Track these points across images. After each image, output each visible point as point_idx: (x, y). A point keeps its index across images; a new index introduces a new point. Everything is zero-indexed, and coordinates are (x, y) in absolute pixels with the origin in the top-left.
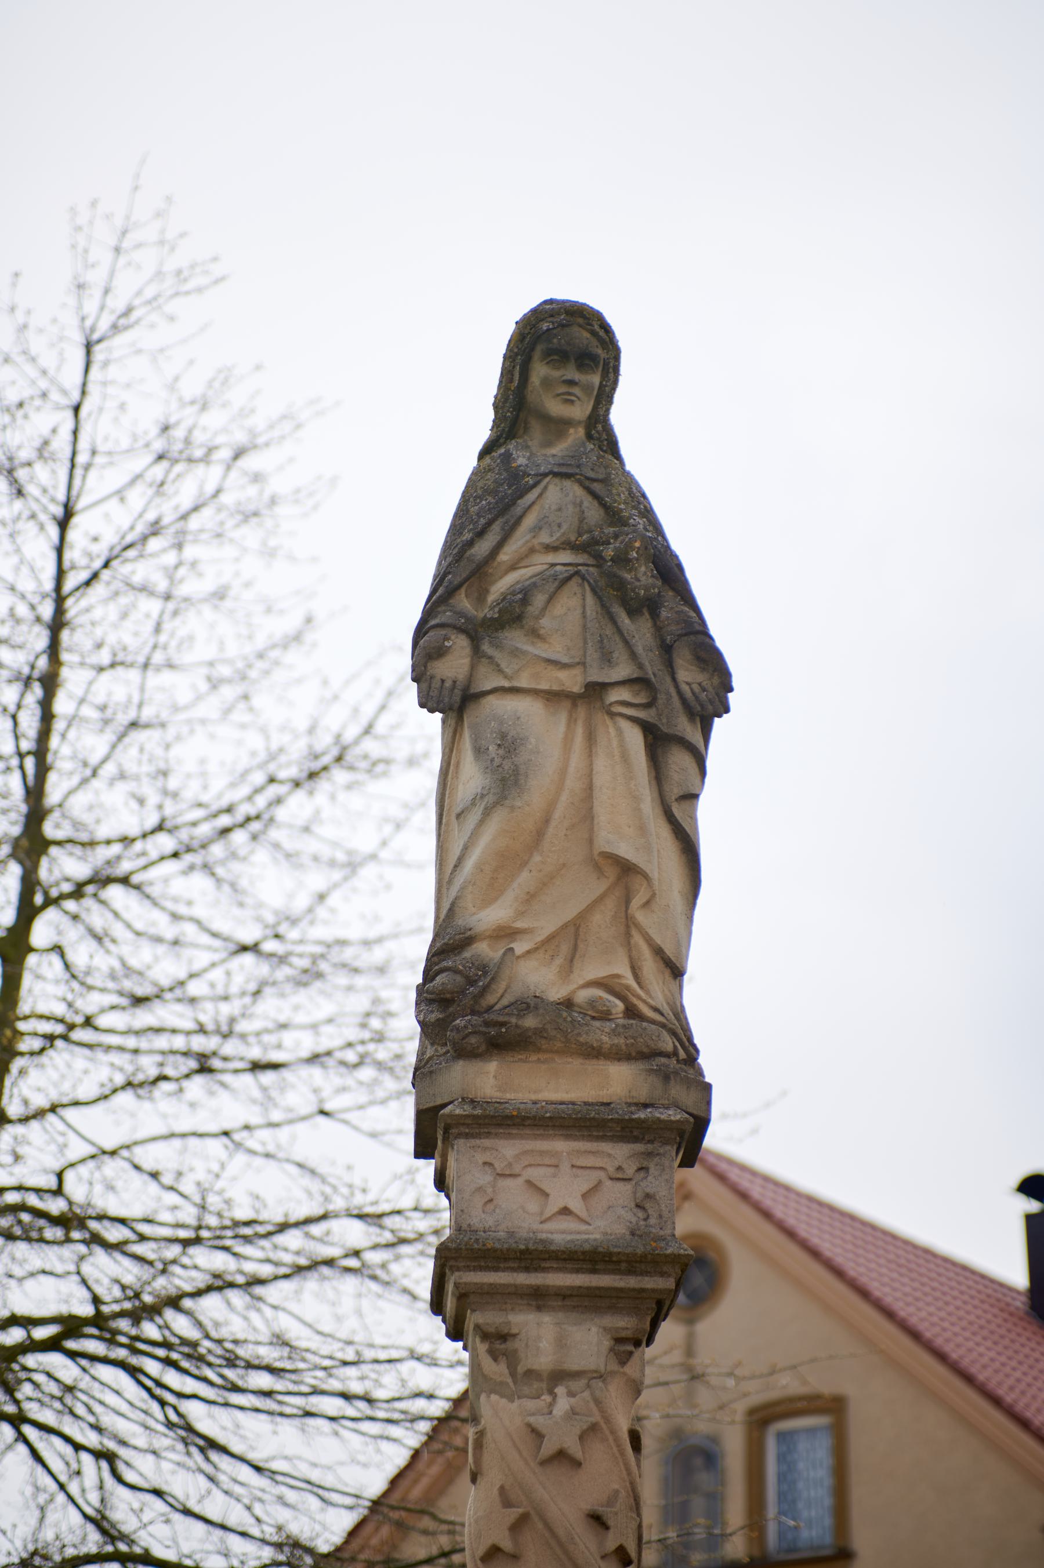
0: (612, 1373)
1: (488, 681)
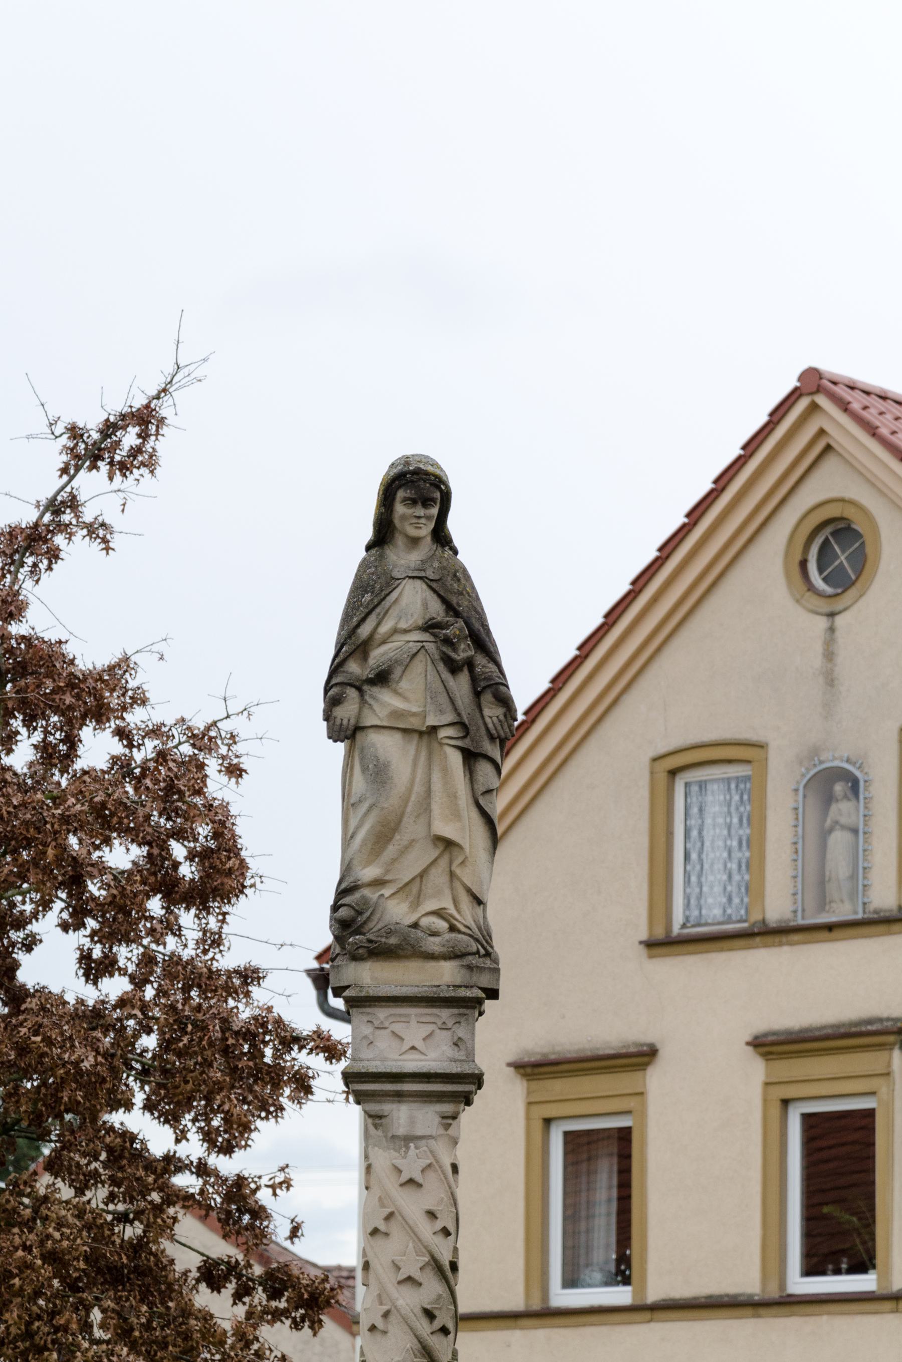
0: (441, 1135)
1: (369, 720)
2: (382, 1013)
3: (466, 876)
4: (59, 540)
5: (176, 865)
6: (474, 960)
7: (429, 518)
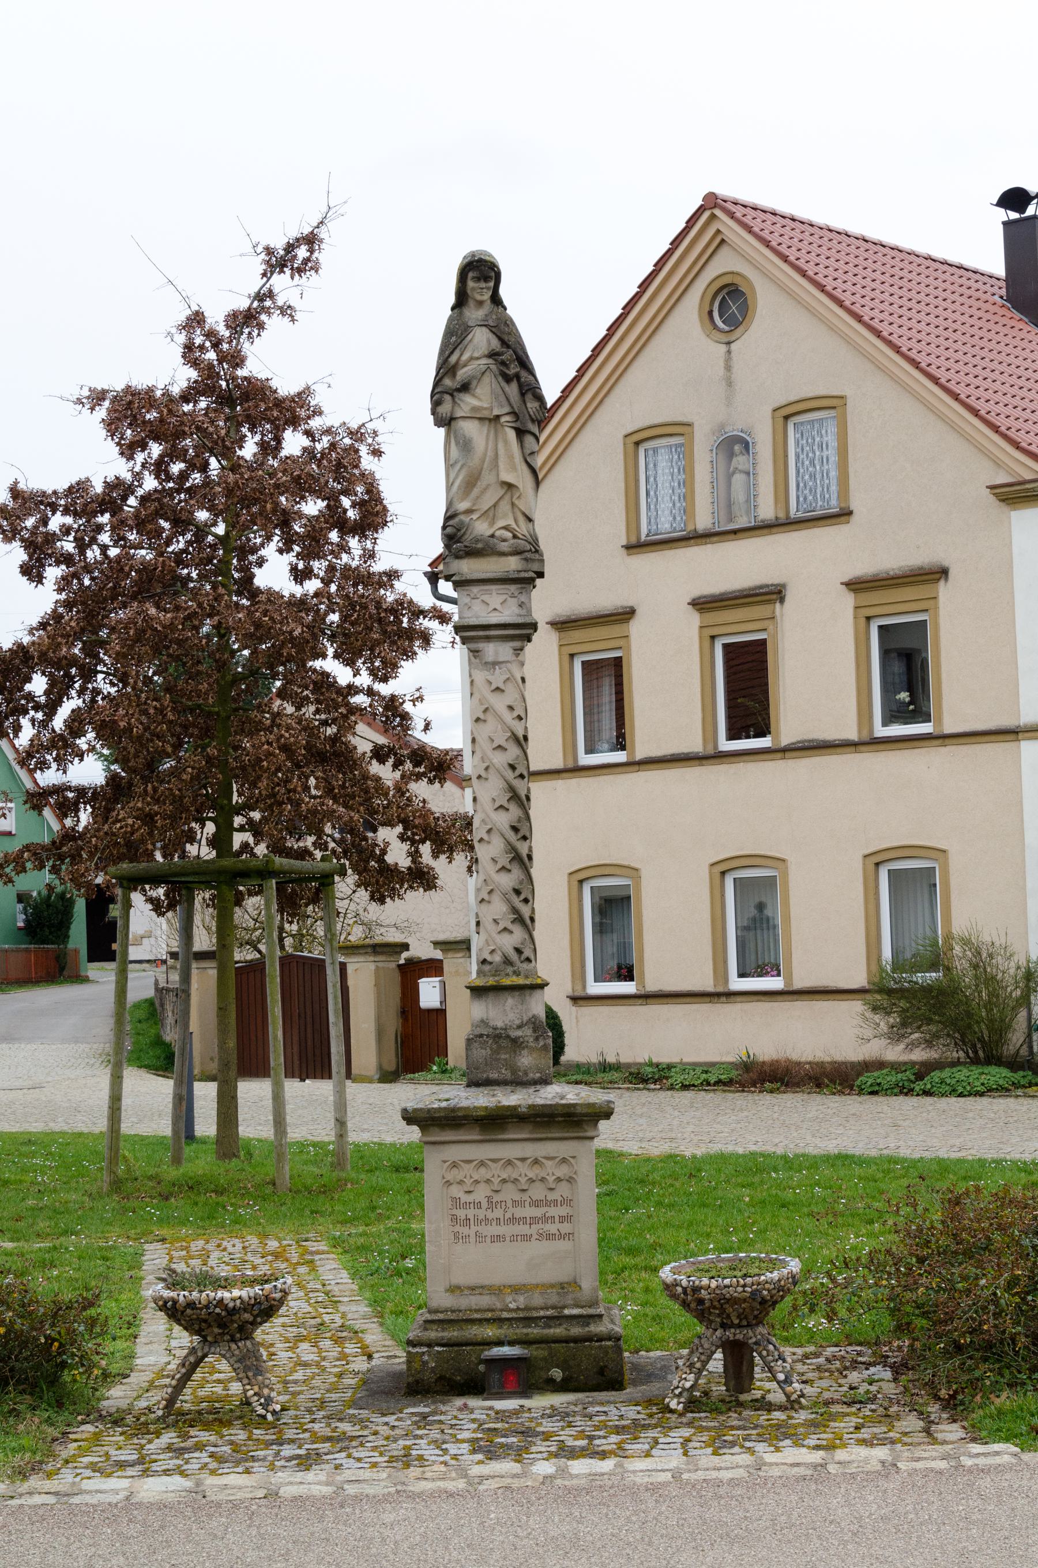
1: (459, 413)
2: (475, 590)
3: (521, 504)
4: (263, 317)
5: (345, 511)
6: (528, 555)
7: (488, 288)
